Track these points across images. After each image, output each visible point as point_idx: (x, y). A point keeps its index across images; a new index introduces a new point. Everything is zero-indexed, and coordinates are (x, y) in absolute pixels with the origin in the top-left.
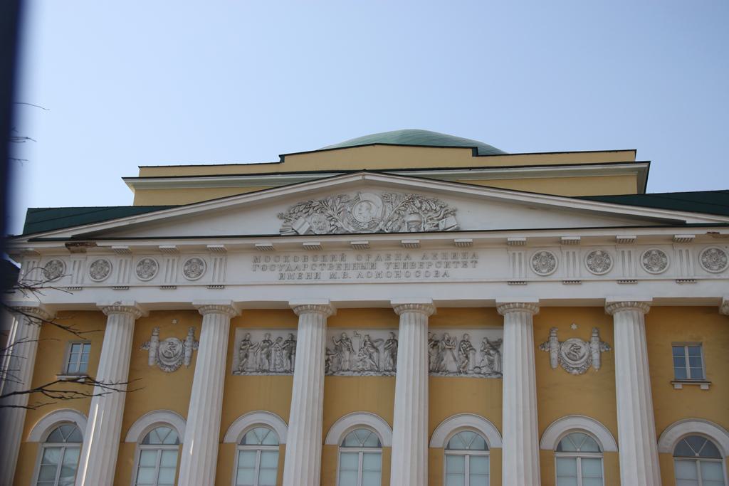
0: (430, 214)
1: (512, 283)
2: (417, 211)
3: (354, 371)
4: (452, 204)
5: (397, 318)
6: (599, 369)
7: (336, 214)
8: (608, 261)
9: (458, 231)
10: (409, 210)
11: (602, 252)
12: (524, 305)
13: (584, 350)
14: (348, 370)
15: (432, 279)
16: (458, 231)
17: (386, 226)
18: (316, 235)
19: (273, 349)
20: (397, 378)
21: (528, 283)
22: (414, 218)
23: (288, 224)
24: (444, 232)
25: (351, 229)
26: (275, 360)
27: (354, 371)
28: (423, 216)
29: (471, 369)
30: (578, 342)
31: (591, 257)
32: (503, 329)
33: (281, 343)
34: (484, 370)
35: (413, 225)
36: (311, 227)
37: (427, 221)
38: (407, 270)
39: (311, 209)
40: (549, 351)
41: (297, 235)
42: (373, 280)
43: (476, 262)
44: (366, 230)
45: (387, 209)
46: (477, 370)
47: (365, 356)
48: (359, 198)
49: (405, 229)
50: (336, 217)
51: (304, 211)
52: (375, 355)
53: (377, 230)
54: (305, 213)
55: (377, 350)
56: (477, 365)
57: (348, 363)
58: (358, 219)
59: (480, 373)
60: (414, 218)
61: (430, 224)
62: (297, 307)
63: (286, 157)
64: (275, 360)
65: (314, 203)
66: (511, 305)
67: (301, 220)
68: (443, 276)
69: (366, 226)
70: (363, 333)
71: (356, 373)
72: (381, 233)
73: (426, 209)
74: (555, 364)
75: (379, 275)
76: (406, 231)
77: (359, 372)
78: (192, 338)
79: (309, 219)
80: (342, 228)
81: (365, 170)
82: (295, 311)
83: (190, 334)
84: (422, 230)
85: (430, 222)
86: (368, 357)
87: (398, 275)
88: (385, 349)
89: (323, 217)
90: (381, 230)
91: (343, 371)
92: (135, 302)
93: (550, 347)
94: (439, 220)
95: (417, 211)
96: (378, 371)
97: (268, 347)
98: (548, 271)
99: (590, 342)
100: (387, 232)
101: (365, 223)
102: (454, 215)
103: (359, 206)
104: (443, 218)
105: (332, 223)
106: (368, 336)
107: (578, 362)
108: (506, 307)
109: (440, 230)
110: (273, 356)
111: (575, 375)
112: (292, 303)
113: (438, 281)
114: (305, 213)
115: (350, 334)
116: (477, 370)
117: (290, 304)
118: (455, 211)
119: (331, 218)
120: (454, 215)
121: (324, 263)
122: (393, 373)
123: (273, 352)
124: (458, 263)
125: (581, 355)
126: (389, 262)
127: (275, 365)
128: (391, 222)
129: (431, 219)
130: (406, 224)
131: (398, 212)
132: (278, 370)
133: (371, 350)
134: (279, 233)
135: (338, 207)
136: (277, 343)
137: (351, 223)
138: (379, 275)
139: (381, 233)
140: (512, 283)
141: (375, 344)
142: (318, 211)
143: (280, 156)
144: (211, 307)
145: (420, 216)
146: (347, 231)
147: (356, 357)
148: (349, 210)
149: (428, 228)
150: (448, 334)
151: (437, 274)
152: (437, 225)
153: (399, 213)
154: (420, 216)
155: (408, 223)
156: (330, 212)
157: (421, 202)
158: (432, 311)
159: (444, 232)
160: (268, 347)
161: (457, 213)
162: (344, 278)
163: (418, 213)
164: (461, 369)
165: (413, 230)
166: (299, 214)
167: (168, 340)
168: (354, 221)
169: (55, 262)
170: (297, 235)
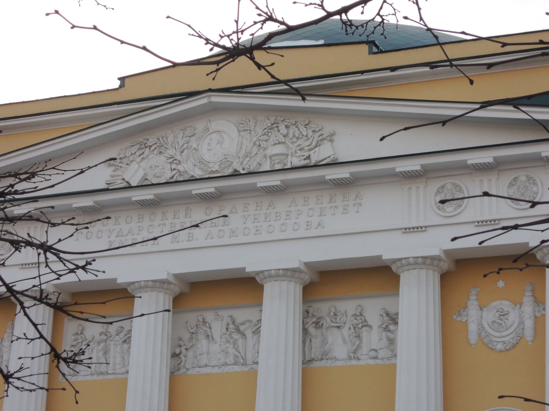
0: (300, 142)
1: (408, 230)
2: (283, 139)
3: (214, 366)
4: (328, 127)
5: (396, 278)
6: (533, 341)
7: (178, 153)
8: (535, 189)
9: (334, 164)
10: (273, 139)
11: (527, 176)
12: (420, 260)
13: (513, 317)
14: (206, 366)
15: (302, 233)
16: (334, 164)
17: (241, 164)
18: (153, 185)
19: (112, 343)
20: (397, 365)
21: (428, 229)
22: (279, 149)
23: (118, 173)
24: (316, 166)
25: (198, 173)
26: (115, 358)
27: (214, 366)
28: (291, 146)
29: (364, 353)
30: (506, 305)
31: (513, 185)
32: (398, 294)
33: (122, 335)
34: (381, 354)
35: (277, 159)
36: (146, 174)
37: (296, 152)
38: (269, 223)
39: (148, 149)
40: (467, 321)
41: (130, 187)
42: (226, 240)
43: (360, 204)
44: (217, 171)
45: (245, 142)
46: (373, 354)
47: (228, 345)
48: (208, 129)
49: (266, 167)
50: (178, 157)
51: (138, 154)
52: (240, 342)
53: (229, 171)
54: (140, 155)
55: (244, 335)
56: (373, 347)
57: (205, 355)
58: (207, 157)
59: (376, 358)
60: (279, 149)
61: (299, 156)
62: (395, 261)
63: (126, 80)
64: (115, 358)
65: (151, 140)
66: (266, 273)
67: (134, 166)
68: (316, 228)
69: (216, 168)
70: (226, 314)
71: (216, 368)
72: (236, 174)
73: (294, 136)
74: (473, 337)
75: (233, 233)
76: (268, 169)
77: (219, 367)
78: (532, 299)
79: (144, 164)
80: (186, 172)
81: (210, 90)
82: (394, 268)
83: (528, 294)
84: (289, 166)
85: (299, 153)
86: (231, 346)
87: (257, 231)
88: (253, 332)
89: (162, 158)
90: (236, 170)
91: (200, 367)
92: (168, 273)
93: (467, 316)
94: (310, 150)
95: (283, 139)
96: (244, 364)
97: (106, 341)
98: (455, 209)
99: (521, 304)
100: (242, 172)
101: (215, 163)
102: (332, 141)
103: (207, 141)
104: (316, 146)
105: (174, 166)
106: (232, 316)
107: (504, 334)
108: (404, 262)
109: (312, 164)
110: (112, 353)
111: (501, 351)
112: (387, 255)
113: (134, 252)
114: (140, 155)
115: (209, 316)
116: (373, 354)
117: (247, 270)
118: (332, 135)
119: (173, 160)
120: (332, 141)
121: (164, 222)
122: (254, 366)
123: (112, 347)
124: (336, 207)
125: (509, 323)
126: (246, 214)
127: (115, 364)
128: (248, 159)
129: (300, 150)
130: (268, 159)
131: (257, 143)
132: (118, 371)
133: (236, 336)
134: (106, 186)
135: (181, 144)
136: (117, 335)
137: (197, 164)
138: (233, 233)
139: (236, 174)
140: (408, 230)
141: (242, 328)
142: (155, 152)
143: (120, 79)
144: (411, 260)
145: (288, 147)
146: (193, 176)
147: (215, 348)
148: (195, 146)
149: (297, 162)
150: (335, 308)
151: (309, 225)
152: (309, 157)
153: (260, 145)
154: (288, 147)
155: (270, 157)
156: (171, 152)
157: (287, 127)
158: (445, 266)
159: (316, 166)
160: (106, 341)
161: (334, 138)
162: (189, 241)
163: (284, 143)
164: (352, 355)
165: (277, 167)
166: (131, 158)
167: (497, 303)
168: (202, 161)
169: (449, 186)
170: (130, 187)
